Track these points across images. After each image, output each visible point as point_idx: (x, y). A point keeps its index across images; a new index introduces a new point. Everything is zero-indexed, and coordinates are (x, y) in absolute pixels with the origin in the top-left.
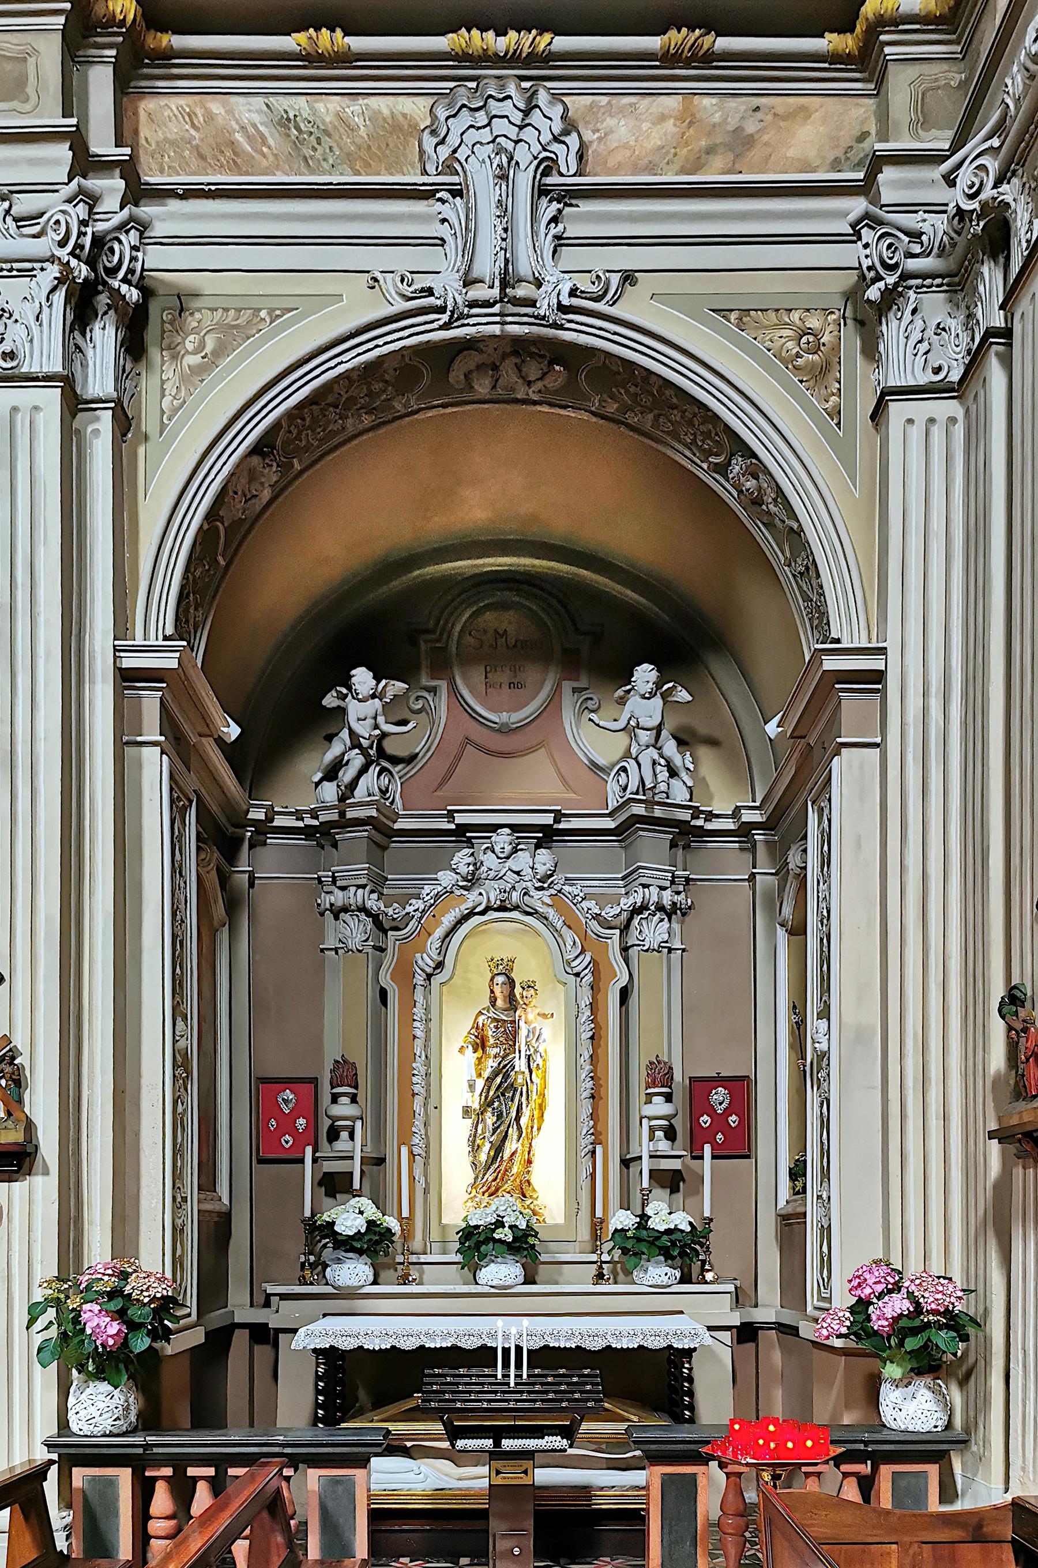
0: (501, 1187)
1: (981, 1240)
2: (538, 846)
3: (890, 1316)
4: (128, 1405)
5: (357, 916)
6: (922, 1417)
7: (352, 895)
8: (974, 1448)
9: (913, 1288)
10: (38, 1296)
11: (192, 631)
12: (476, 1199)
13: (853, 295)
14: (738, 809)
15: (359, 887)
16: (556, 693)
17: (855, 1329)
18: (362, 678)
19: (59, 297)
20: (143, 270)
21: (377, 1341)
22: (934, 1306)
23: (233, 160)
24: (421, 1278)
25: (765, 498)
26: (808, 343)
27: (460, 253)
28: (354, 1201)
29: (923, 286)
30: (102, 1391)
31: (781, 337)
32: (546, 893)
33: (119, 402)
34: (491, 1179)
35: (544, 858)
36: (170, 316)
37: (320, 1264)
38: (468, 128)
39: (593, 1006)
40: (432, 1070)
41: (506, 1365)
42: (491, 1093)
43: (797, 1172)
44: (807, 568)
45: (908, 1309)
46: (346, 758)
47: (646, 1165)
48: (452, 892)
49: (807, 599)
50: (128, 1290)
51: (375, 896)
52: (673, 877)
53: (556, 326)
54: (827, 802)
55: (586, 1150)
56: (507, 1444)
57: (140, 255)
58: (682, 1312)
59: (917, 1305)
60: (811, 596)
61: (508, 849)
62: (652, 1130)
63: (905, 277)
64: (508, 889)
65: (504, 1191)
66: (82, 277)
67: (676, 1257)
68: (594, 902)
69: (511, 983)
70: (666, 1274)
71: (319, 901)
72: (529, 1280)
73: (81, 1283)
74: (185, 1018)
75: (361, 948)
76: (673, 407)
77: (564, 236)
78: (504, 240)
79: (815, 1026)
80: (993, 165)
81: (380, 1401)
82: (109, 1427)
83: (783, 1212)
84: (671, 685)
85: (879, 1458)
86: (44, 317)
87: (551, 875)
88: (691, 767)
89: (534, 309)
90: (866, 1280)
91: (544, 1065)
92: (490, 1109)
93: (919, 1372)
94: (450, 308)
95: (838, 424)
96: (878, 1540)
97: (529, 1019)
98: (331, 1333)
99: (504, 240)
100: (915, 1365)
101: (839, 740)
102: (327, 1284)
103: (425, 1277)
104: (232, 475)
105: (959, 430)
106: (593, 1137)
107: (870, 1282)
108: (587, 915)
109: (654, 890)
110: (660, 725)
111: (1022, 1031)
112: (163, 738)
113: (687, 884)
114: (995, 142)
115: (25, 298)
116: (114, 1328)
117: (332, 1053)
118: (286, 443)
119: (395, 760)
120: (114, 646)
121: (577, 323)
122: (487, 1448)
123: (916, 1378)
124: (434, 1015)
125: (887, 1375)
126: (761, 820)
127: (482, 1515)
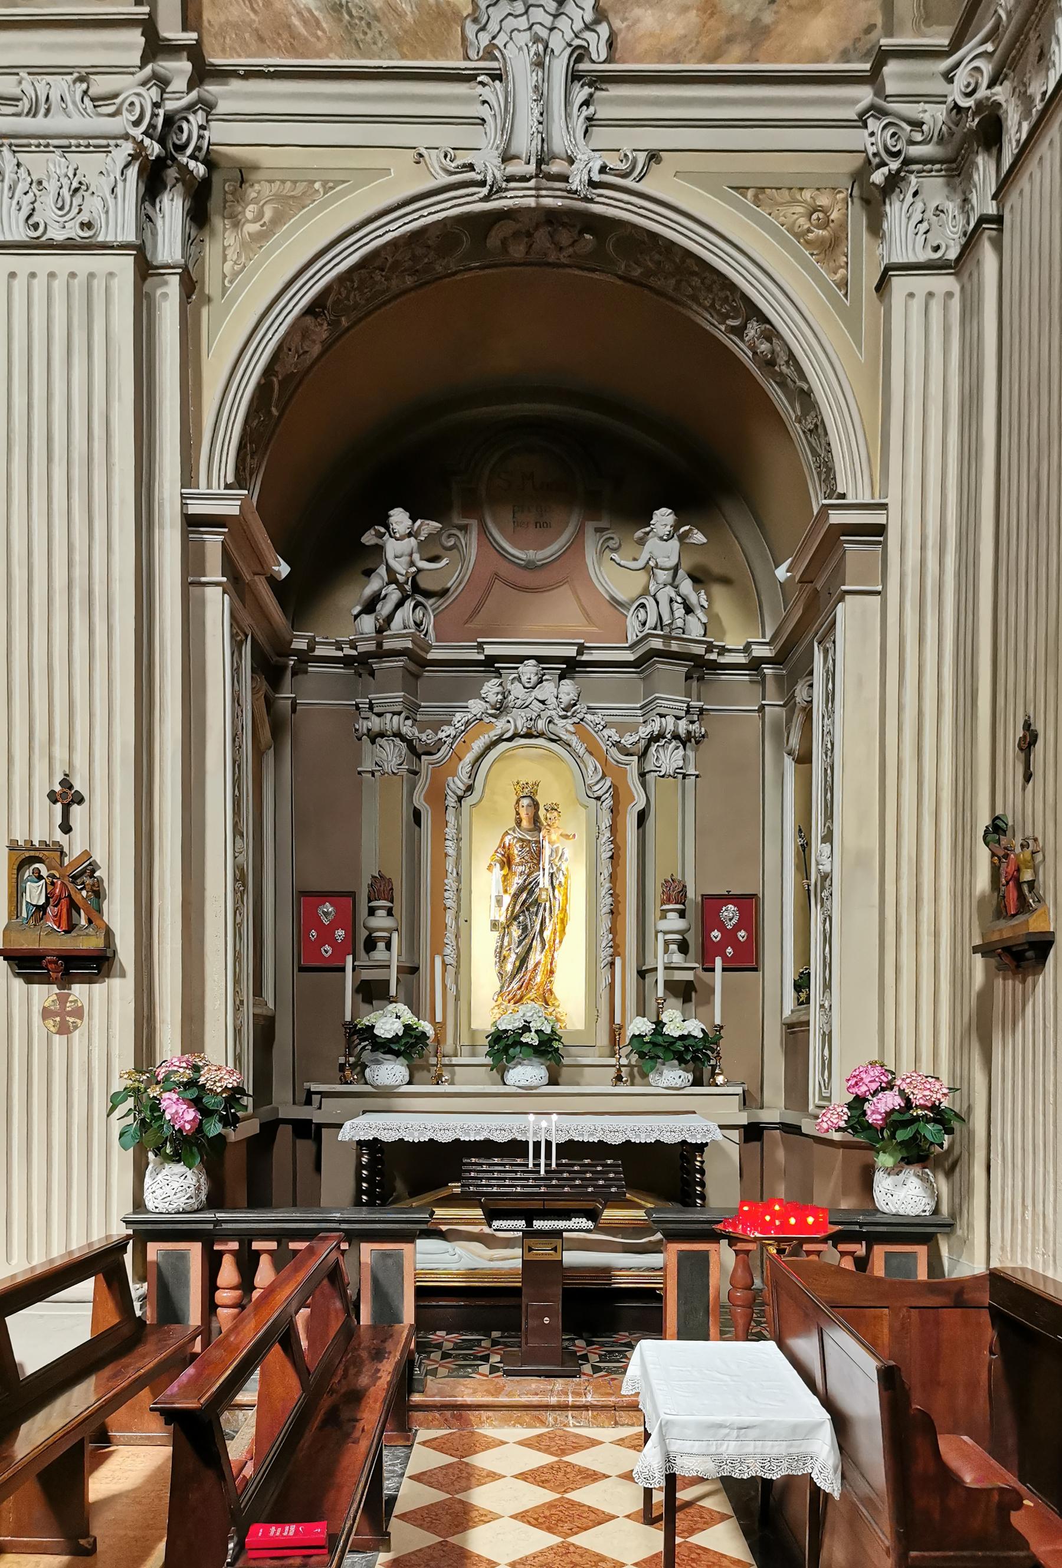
0: (525, 995)
1: (966, 1046)
2: (562, 677)
3: (883, 1111)
4: (200, 1185)
5: (393, 741)
6: (912, 1202)
7: (388, 722)
8: (959, 1232)
9: (904, 1086)
10: (117, 1086)
11: (248, 477)
12: (503, 1007)
13: (860, 176)
14: (748, 645)
15: (394, 713)
16: (580, 533)
17: (852, 1122)
18: (399, 518)
19: (133, 172)
20: (209, 144)
21: (416, 1134)
22: (922, 1102)
23: (291, 44)
24: (452, 1078)
25: (778, 360)
26: (819, 219)
27: (499, 132)
28: (391, 1007)
29: (924, 171)
30: (176, 1172)
31: (794, 213)
32: (570, 721)
33: (185, 268)
34: (516, 987)
35: (568, 689)
36: (231, 188)
37: (360, 1065)
38: (506, 17)
39: (613, 828)
40: (462, 886)
41: (537, 1155)
42: (517, 908)
43: (802, 984)
44: (816, 426)
45: (899, 1105)
46: (383, 593)
47: (661, 976)
48: (481, 720)
49: (815, 453)
50: (202, 1080)
51: (409, 722)
52: (688, 707)
53: (586, 199)
54: (831, 644)
55: (606, 961)
56: (538, 1224)
57: (206, 133)
58: (694, 1112)
59: (908, 1101)
60: (820, 452)
61: (534, 679)
62: (667, 943)
63: (907, 162)
64: (534, 717)
65: (528, 999)
66: (155, 154)
67: (689, 1061)
68: (614, 730)
69: (536, 805)
70: (680, 1077)
71: (357, 727)
72: (553, 1081)
73: (158, 1074)
74: (242, 835)
75: (395, 771)
76: (694, 274)
77: (596, 117)
78: (540, 123)
79: (818, 848)
80: (987, 68)
81: (416, 1190)
82: (182, 1205)
83: (788, 1021)
84: (687, 528)
85: (872, 1239)
86: (119, 190)
87: (575, 705)
88: (706, 604)
89: (567, 184)
90: (862, 1079)
91: (567, 882)
92: (516, 923)
93: (908, 1161)
94: (489, 182)
95: (846, 295)
96: (873, 1304)
97: (551, 840)
98: (374, 1126)
99: (540, 123)
100: (905, 1155)
101: (843, 588)
102: (366, 1083)
103: (457, 1078)
104: (287, 334)
105: (956, 303)
106: (612, 950)
107: (866, 1081)
108: (608, 742)
109: (670, 720)
110: (677, 565)
111: (1003, 857)
112: (225, 579)
113: (701, 714)
114: (989, 47)
115: (101, 172)
116: (191, 1114)
117: (369, 869)
118: (337, 302)
119: (428, 594)
120: (181, 494)
121: (607, 197)
122: (520, 1228)
123: (906, 1166)
124: (464, 835)
125: (880, 1165)
126: (770, 655)
127: (515, 1292)
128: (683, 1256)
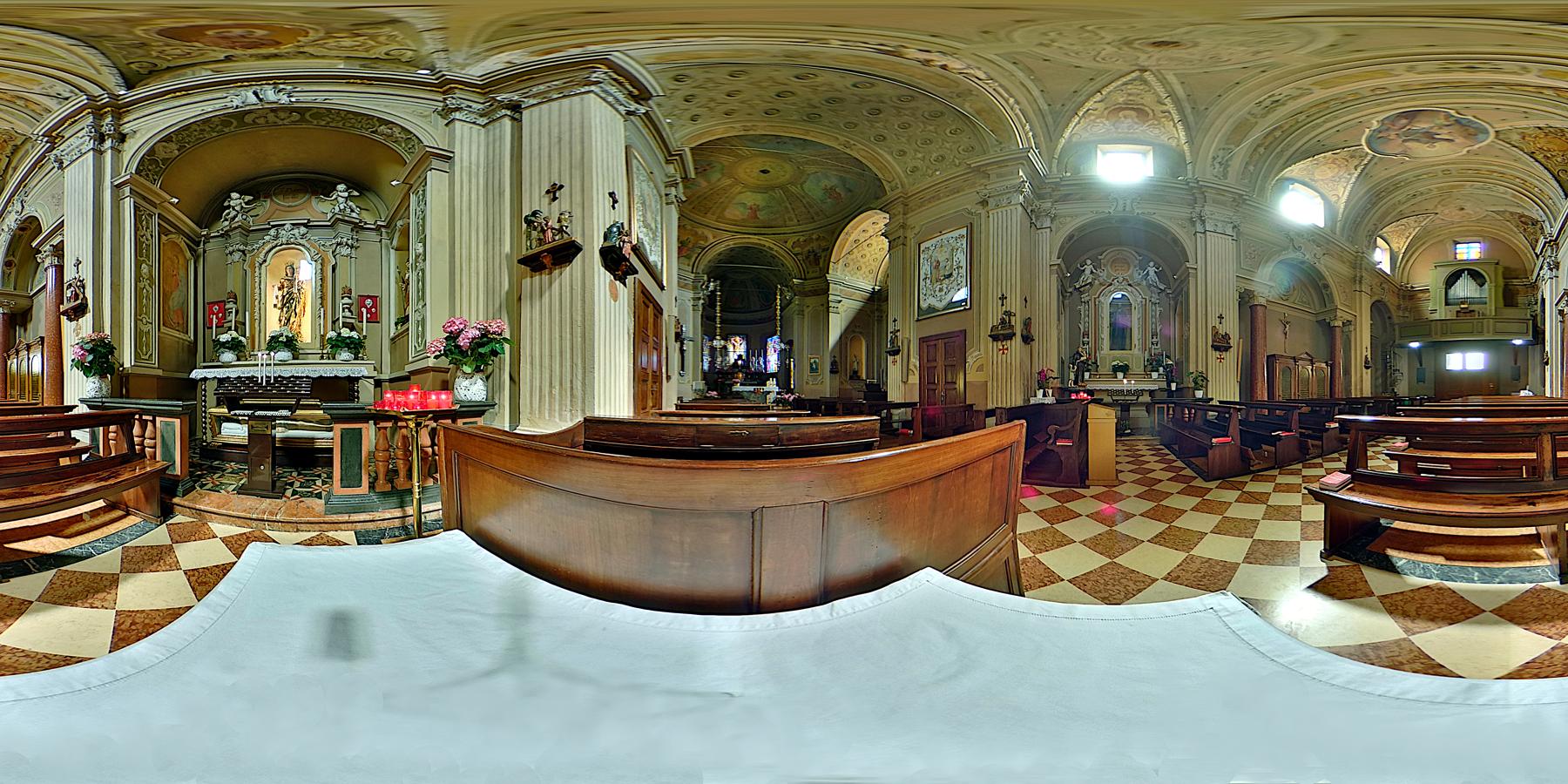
56: (1025, 121)
128: (344, 433)
